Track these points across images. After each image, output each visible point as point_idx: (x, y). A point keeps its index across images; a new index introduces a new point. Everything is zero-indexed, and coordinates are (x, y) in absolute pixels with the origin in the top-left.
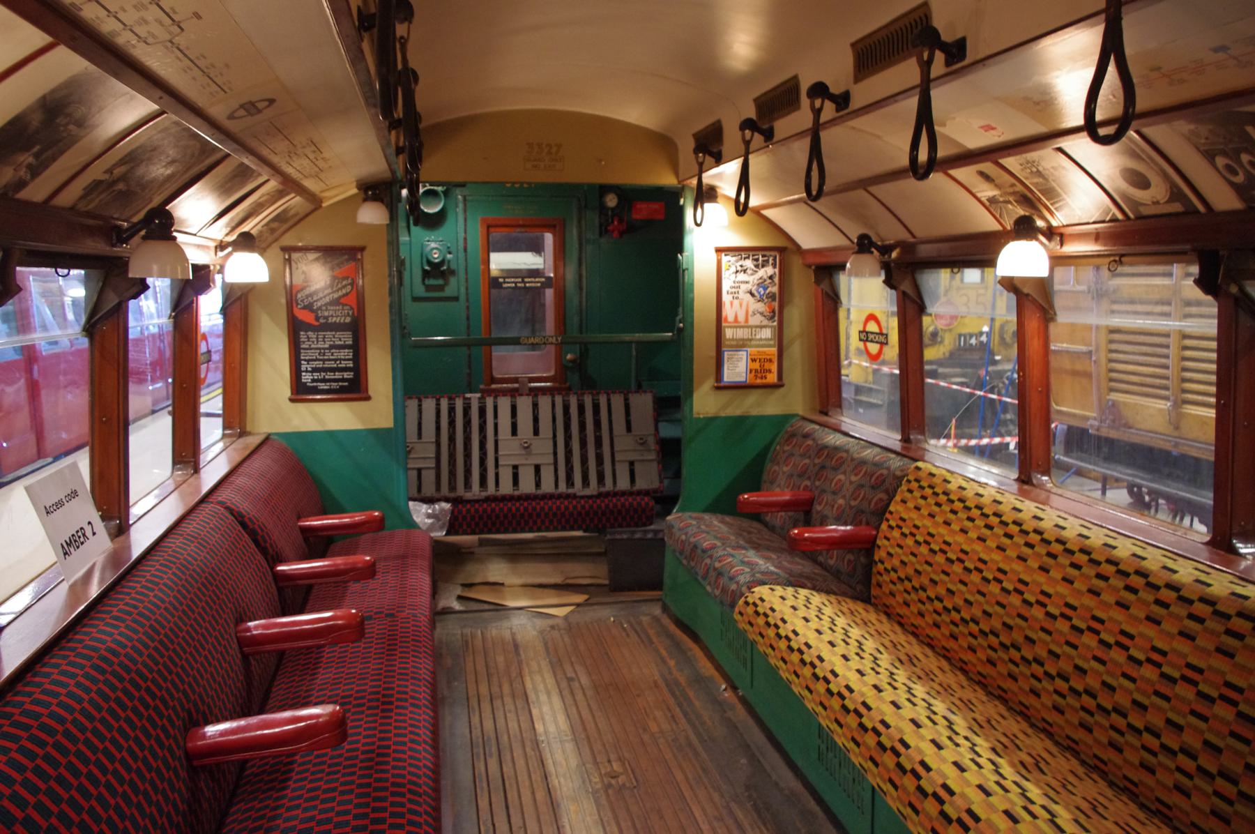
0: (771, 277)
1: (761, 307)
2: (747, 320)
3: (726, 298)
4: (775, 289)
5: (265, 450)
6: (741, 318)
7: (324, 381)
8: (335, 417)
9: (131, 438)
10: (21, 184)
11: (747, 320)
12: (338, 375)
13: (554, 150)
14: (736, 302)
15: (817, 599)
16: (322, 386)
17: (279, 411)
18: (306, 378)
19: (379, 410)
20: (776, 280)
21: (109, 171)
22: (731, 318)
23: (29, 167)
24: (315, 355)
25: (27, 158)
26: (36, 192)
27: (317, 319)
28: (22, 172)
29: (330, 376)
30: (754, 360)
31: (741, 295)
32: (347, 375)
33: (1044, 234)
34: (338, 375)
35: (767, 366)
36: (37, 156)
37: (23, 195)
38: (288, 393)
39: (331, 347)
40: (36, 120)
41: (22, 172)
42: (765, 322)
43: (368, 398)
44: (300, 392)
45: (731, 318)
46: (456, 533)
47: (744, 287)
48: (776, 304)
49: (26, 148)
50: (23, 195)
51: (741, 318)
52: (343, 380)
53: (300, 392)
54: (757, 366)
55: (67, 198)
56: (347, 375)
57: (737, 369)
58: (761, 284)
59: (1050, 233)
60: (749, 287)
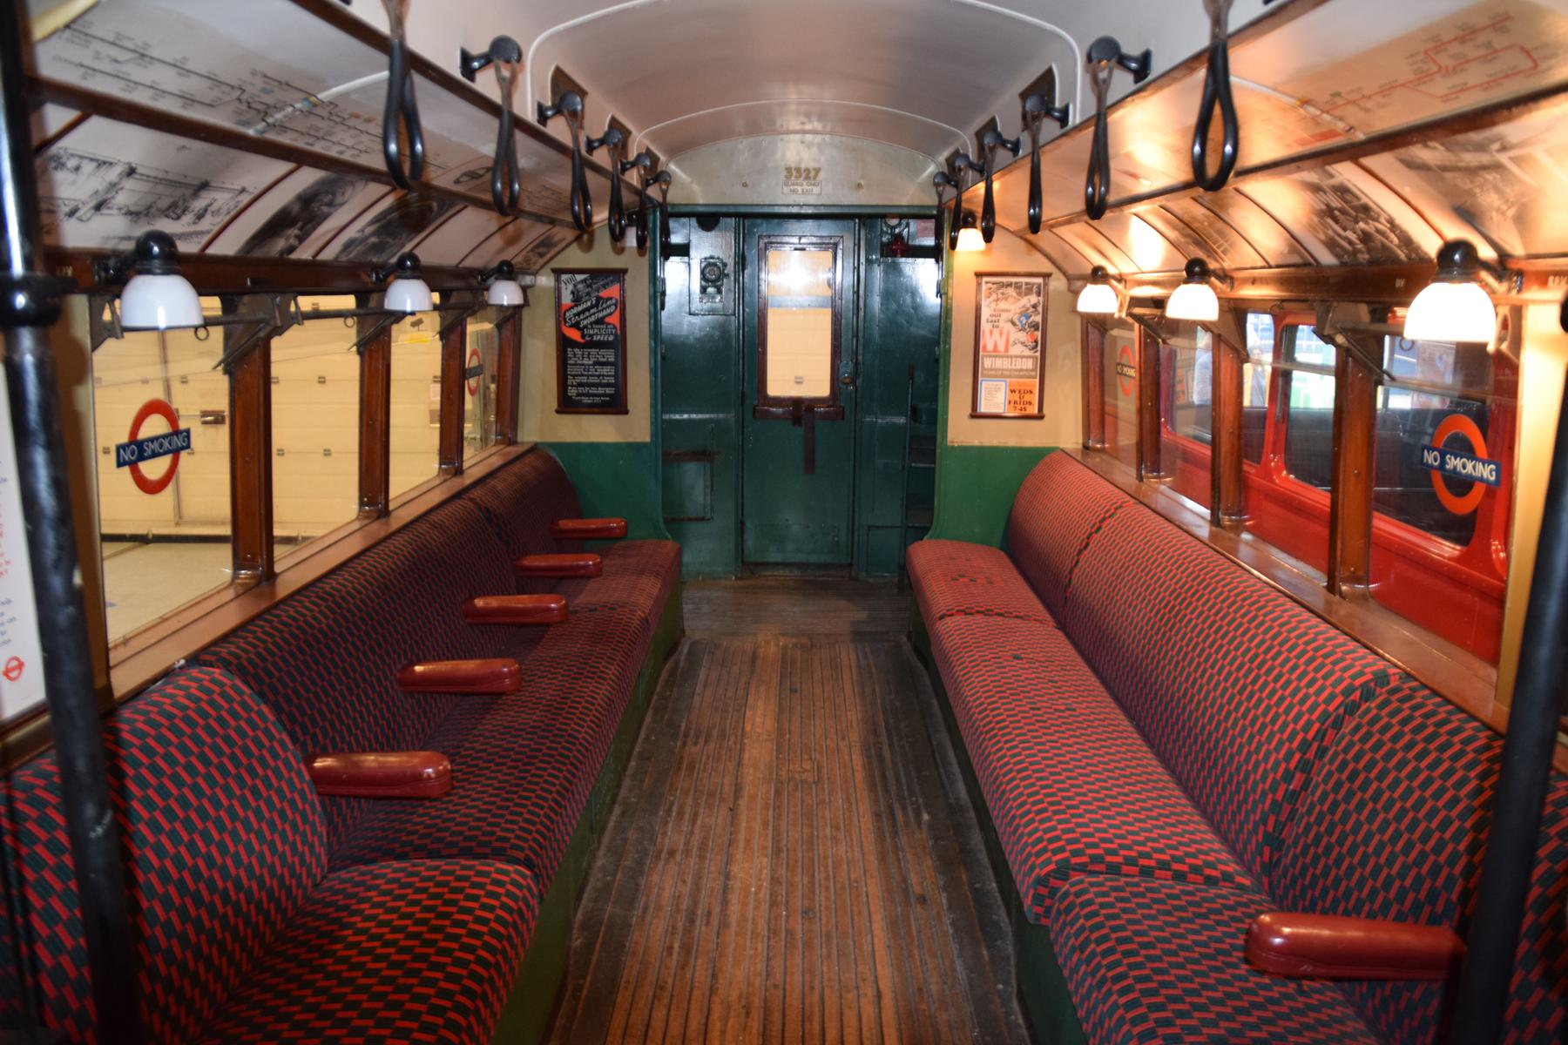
0: (1034, 306)
1: (1022, 336)
2: (1007, 350)
3: (985, 326)
4: (1038, 319)
5: (530, 459)
6: (1001, 348)
7: (588, 395)
8: (598, 430)
9: (1332, 394)
10: (292, 249)
11: (1007, 350)
12: (601, 390)
13: (812, 174)
14: (996, 331)
15: (687, 607)
16: (586, 400)
17: (541, 423)
18: (572, 392)
19: (635, 426)
20: (1040, 309)
21: (362, 231)
22: (990, 347)
23: (297, 237)
24: (580, 370)
25: (295, 231)
26: (304, 253)
27: (583, 336)
28: (292, 241)
29: (593, 391)
30: (1013, 391)
31: (1002, 324)
32: (609, 391)
33: (1219, 277)
34: (601, 390)
35: (1027, 397)
36: (301, 229)
37: (294, 256)
38: (555, 406)
39: (596, 363)
40: (296, 208)
41: (292, 241)
42: (1027, 353)
43: (626, 412)
44: (567, 405)
45: (990, 347)
46: (1496, 629)
47: (1004, 316)
48: (1039, 334)
49: (292, 225)
50: (294, 256)
51: (1001, 348)
52: (605, 395)
53: (567, 405)
54: (1016, 397)
55: (328, 255)
56: (609, 391)
57: (994, 398)
58: (1024, 313)
59: (1225, 276)
60: (1010, 315)
